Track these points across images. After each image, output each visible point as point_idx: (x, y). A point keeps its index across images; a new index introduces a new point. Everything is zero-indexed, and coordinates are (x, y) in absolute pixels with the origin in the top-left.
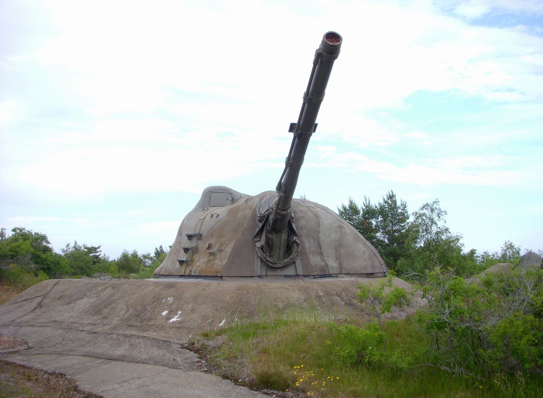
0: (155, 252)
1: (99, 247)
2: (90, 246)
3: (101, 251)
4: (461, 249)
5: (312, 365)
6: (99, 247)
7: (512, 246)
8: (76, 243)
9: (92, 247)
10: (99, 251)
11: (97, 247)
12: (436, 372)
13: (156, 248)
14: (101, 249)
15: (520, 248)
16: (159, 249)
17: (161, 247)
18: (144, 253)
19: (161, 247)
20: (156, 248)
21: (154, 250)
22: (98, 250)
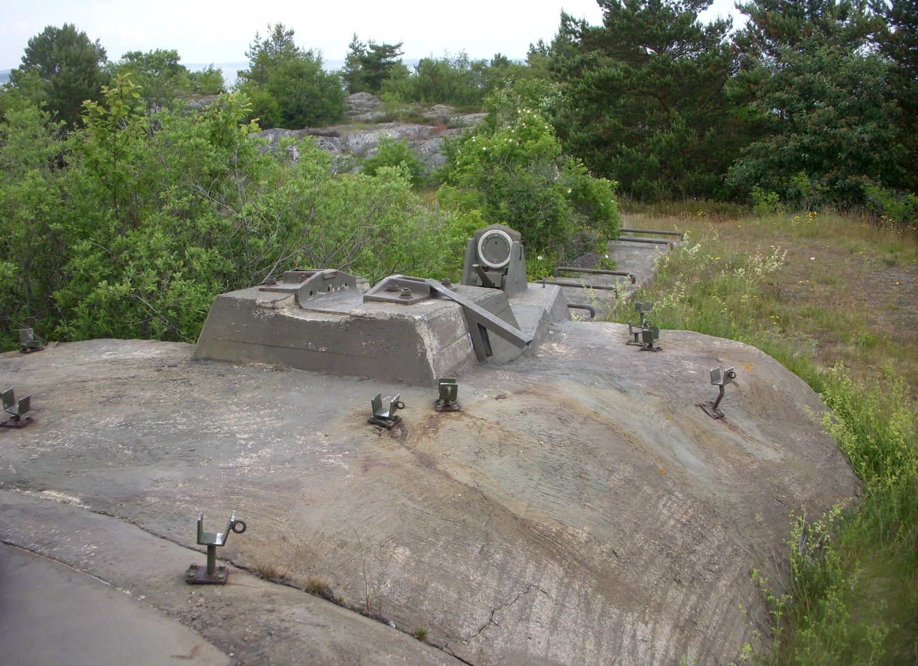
0: (528, 53)
1: (399, 46)
2: (380, 45)
3: (402, 53)
4: (242, 81)
5: (789, 234)
6: (399, 46)
7: (782, 83)
8: (355, 38)
9: (385, 46)
10: (399, 53)
11: (393, 45)
12: (640, 459)
13: (531, 45)
14: (402, 49)
15: (465, 52)
16: (536, 47)
17: (541, 42)
18: (437, 55)
19: (541, 42)
20: (531, 45)
21: (527, 49)
22: (397, 51)
